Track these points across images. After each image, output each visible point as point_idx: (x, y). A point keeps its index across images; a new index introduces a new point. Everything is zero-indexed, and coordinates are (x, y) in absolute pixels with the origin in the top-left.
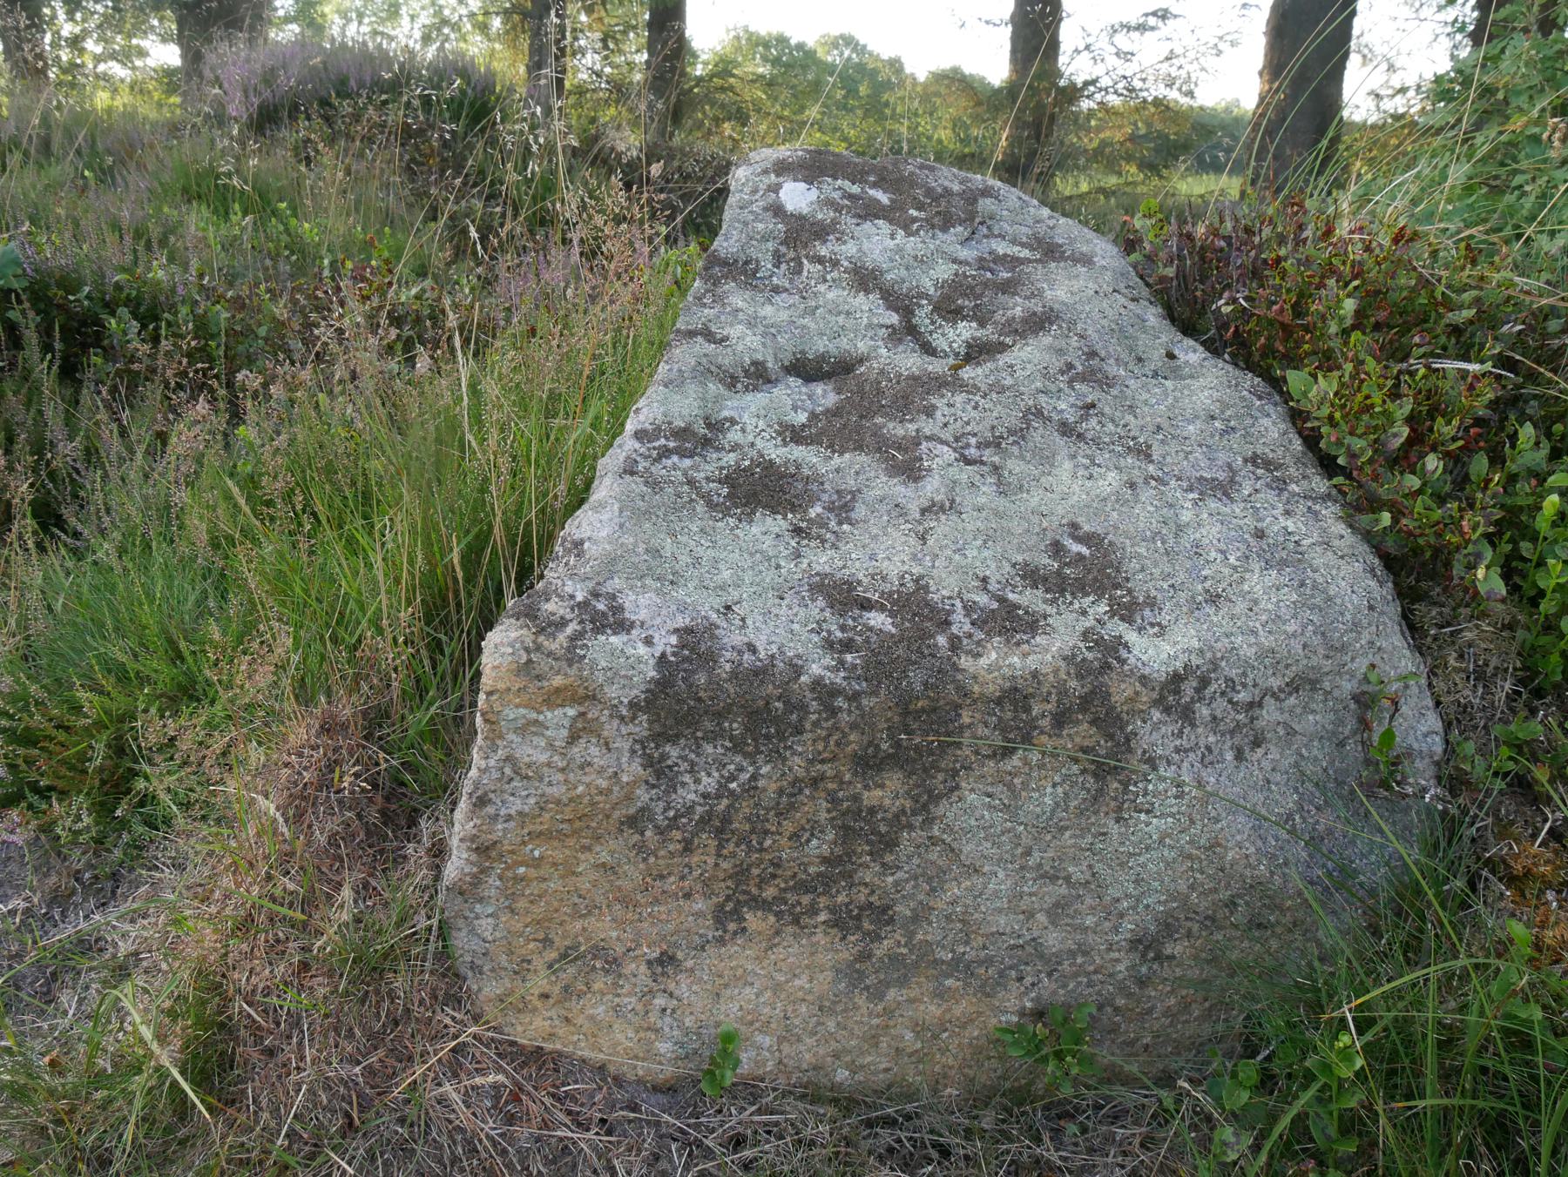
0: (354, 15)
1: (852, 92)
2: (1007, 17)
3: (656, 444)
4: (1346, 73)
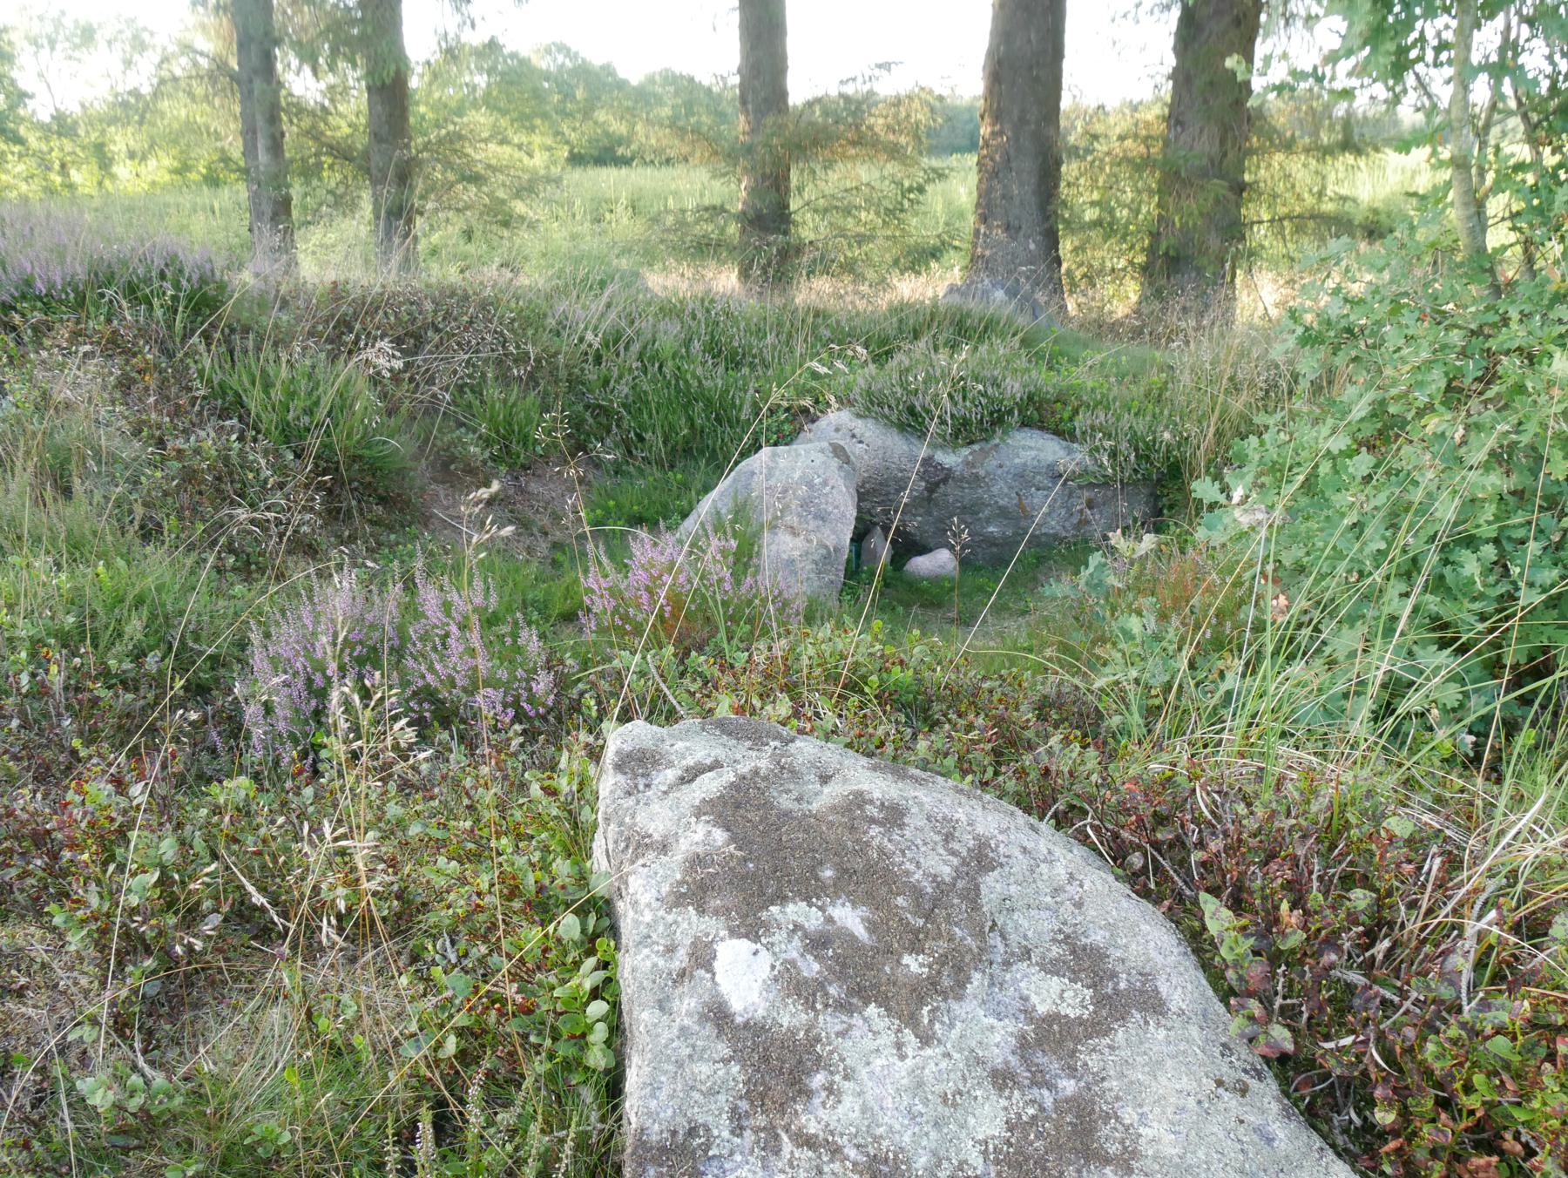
0: (45, 42)
1: (568, 96)
2: (735, 70)
4: (1067, 65)
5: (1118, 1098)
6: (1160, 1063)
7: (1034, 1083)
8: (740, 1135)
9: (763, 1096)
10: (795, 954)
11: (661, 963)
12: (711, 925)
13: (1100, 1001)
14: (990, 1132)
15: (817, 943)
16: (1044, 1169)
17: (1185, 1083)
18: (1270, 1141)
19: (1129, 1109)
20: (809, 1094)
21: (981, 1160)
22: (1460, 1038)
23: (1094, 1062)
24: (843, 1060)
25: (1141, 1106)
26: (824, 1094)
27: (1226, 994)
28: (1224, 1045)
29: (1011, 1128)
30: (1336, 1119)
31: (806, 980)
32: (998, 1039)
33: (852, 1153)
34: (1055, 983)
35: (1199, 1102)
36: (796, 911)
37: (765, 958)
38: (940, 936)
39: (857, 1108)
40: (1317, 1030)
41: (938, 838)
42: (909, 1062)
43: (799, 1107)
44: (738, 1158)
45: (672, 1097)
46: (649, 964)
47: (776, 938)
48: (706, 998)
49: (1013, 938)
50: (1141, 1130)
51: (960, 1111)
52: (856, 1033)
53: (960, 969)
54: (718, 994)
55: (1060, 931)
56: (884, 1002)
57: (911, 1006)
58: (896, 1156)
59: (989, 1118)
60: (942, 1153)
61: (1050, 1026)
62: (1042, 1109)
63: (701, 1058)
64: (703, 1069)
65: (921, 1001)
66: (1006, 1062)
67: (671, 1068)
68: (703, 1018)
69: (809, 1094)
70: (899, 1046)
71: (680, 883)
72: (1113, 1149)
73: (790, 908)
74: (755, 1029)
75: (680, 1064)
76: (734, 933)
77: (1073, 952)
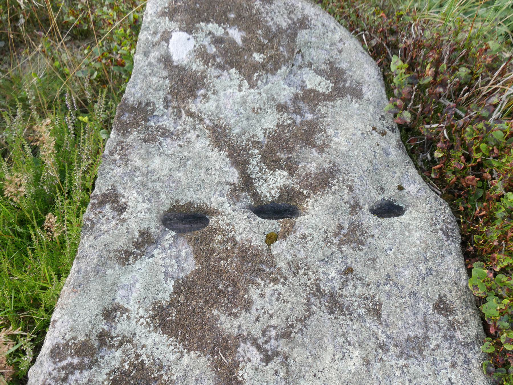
3: (64, 363)
5: (328, 125)
6: (351, 116)
7: (294, 112)
8: (167, 109)
9: (177, 94)
10: (206, 43)
11: (150, 38)
12: (173, 25)
13: (334, 89)
14: (269, 126)
15: (217, 41)
16: (287, 144)
17: (360, 126)
18: (388, 154)
19: (332, 130)
20: (196, 97)
21: (263, 136)
22: (482, 129)
23: (323, 110)
24: (214, 86)
25: (337, 130)
26: (202, 98)
27: (389, 92)
28: (382, 116)
29: (278, 126)
30: (421, 155)
31: (207, 54)
32: (285, 93)
33: (207, 122)
34: (319, 78)
35: (363, 134)
36: (212, 27)
37: (192, 42)
38: (272, 48)
39: (214, 106)
40: (426, 118)
41: (286, 12)
42: (242, 93)
43: (190, 101)
44: (165, 117)
45: (141, 89)
46: (145, 37)
47: (200, 35)
48: (163, 53)
49: (307, 58)
50: (334, 138)
51: (259, 116)
52: (223, 78)
53: (277, 63)
54: (168, 52)
55: (328, 60)
56: (239, 68)
57: (249, 72)
58: (225, 126)
59: (270, 121)
60: (247, 130)
61: (310, 93)
62: (294, 122)
63: (155, 75)
64: (155, 80)
65: (255, 71)
66: (286, 102)
67: (142, 77)
68: (159, 61)
69: (196, 97)
70: (240, 86)
71: (165, 8)
72: (319, 142)
73: (210, 25)
74: (181, 69)
75: (146, 76)
76: (181, 29)
77: (331, 69)
